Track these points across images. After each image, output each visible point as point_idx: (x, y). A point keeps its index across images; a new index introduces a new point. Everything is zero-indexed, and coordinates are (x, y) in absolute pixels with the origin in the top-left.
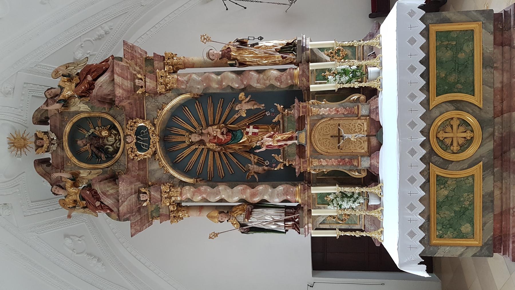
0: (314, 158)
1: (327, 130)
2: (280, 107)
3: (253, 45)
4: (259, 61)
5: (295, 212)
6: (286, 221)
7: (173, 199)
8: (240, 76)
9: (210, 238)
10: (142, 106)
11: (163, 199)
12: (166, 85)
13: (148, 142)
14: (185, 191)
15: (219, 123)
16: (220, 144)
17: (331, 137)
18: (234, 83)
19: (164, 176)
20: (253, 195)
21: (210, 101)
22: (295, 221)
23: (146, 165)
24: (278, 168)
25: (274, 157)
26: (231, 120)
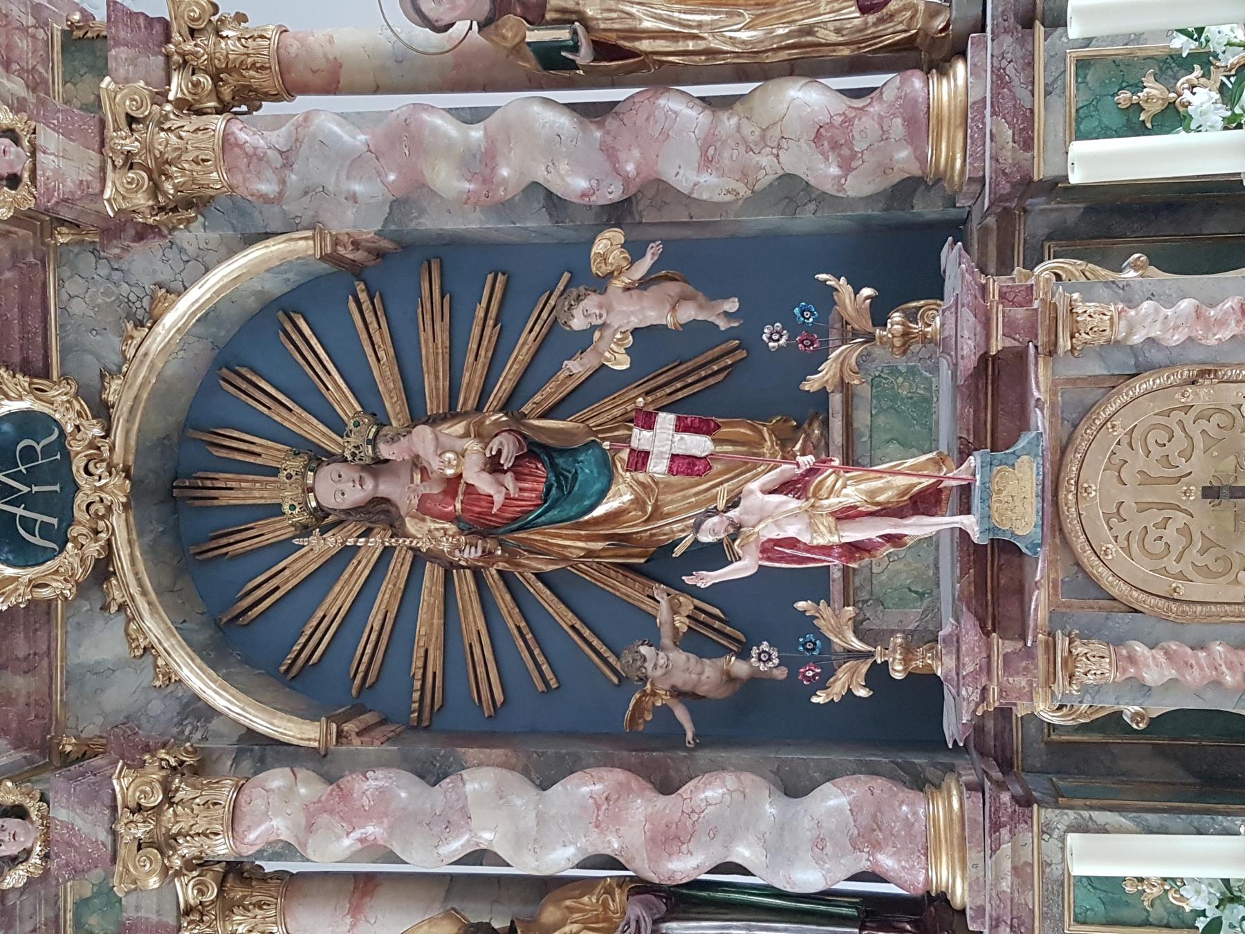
0: (1086, 637)
1: (1173, 449)
2: (853, 300)
4: (714, 29)
7: (187, 849)
8: (601, 125)
10: (35, 299)
11: (122, 852)
12: (158, 172)
13: (63, 506)
14: (259, 804)
15: (479, 408)
16: (479, 524)
17: (1210, 493)
18: (564, 167)
19: (156, 707)
20: (668, 839)
21: (431, 288)
23: (50, 640)
26: (550, 393)
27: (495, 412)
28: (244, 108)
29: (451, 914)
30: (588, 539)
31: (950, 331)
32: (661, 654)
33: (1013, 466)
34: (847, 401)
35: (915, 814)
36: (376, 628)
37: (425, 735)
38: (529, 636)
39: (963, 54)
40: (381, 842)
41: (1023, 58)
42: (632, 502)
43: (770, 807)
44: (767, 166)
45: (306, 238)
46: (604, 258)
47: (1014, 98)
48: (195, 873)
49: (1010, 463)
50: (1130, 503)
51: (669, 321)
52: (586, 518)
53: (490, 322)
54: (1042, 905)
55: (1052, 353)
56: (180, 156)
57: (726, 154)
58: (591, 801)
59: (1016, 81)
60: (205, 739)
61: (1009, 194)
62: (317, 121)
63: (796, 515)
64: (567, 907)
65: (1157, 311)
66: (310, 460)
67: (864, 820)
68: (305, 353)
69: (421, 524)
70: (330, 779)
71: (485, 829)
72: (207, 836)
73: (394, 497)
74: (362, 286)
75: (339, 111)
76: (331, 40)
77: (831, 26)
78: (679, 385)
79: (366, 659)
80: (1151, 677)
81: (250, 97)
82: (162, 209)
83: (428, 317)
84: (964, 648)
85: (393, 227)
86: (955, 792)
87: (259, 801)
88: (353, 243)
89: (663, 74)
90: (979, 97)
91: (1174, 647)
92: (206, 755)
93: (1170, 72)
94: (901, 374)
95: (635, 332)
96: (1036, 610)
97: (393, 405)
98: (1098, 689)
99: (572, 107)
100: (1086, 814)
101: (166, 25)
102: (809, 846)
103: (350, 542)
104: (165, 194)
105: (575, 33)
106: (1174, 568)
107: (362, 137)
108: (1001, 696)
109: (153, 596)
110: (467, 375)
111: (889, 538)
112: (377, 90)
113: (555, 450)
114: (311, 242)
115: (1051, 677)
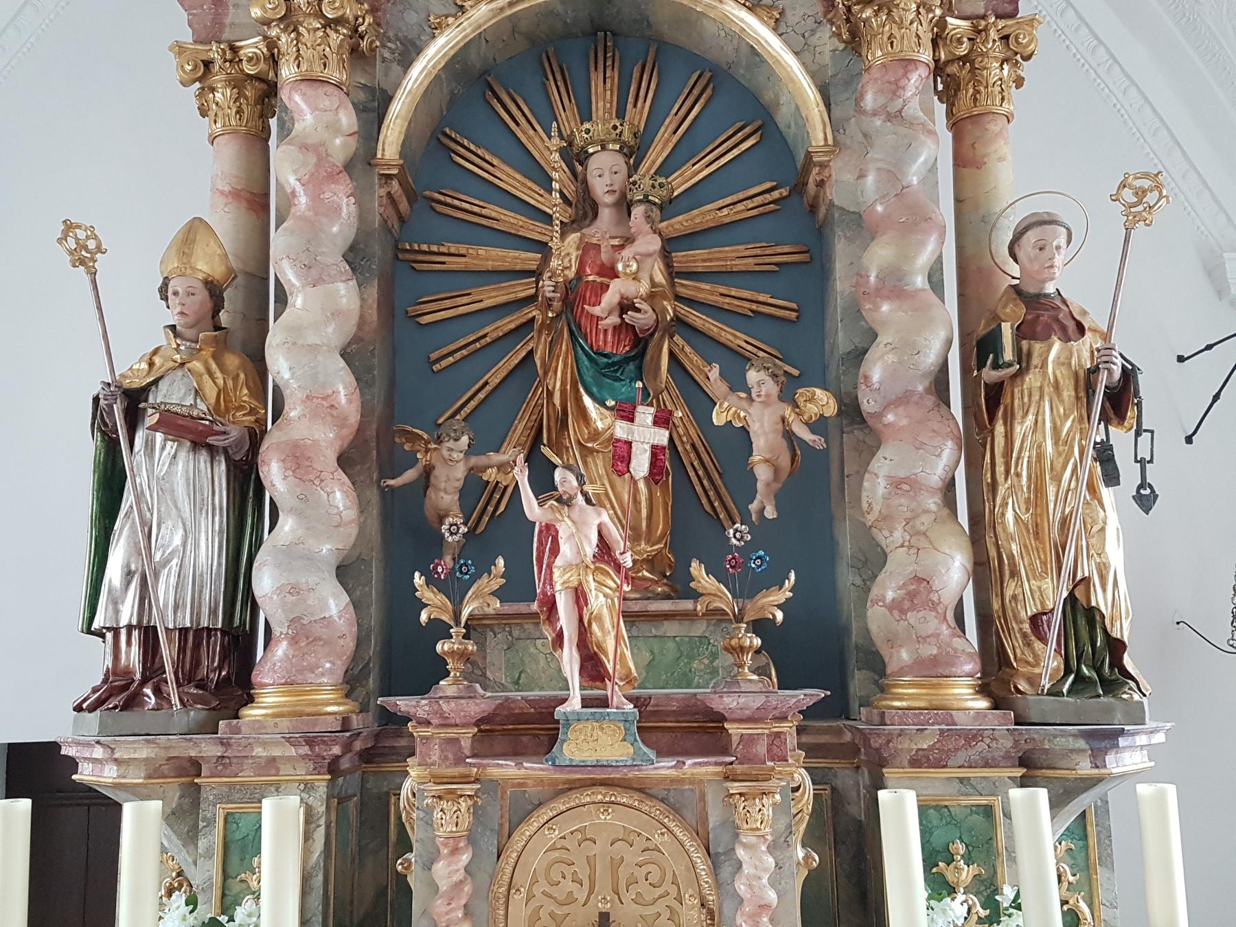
0: (476, 811)
1: (643, 887)
2: (773, 603)
3: (1105, 455)
5: (201, 685)
6: (149, 637)
7: (285, 40)
8: (928, 391)
9: (69, 227)
14: (326, 103)
15: (678, 298)
16: (574, 295)
18: (891, 358)
20: (298, 459)
21: (784, 253)
22: (144, 682)
24: (426, 593)
25: (485, 567)
26: (692, 359)
27: (674, 310)
28: (940, 87)
29: (231, 275)
30: (563, 392)
31: (745, 687)
32: (462, 455)
33: (624, 740)
34: (686, 615)
35: (323, 674)
36: (484, 212)
37: (390, 254)
38: (478, 345)
39: (995, 706)
40: (293, 210)
41: (993, 758)
42: (596, 430)
43: (327, 549)
44: (893, 538)
45: (826, 139)
46: (811, 400)
47: (957, 750)
48: (265, 50)
49: (628, 737)
50: (595, 850)
51: (756, 458)
52: (582, 390)
53: (754, 307)
54: (242, 784)
55: (727, 778)
56: (895, 22)
57: (903, 501)
58: (330, 392)
59: (971, 752)
60: (384, 60)
61: (870, 747)
62: (929, 141)
63: (579, 553)
64: (238, 376)
65: (766, 870)
66: (631, 147)
67: (318, 630)
68: (725, 145)
69: (574, 246)
70: (348, 167)
71: (305, 300)
72: (297, 58)
73: (598, 223)
74: (785, 194)
75: (939, 165)
76: (1001, 159)
77: (1019, 590)
78: (701, 473)
79: (456, 203)
80: (440, 868)
81: (950, 93)
82: (849, 9)
83: (759, 252)
84: (463, 701)
85: (836, 215)
86: (341, 708)
87: (327, 103)
88: (822, 180)
89: (975, 446)
90: (956, 719)
91: (466, 889)
92: (368, 61)
93: (982, 888)
94: (712, 662)
95: (745, 431)
96: (501, 766)
97: (680, 222)
98: (429, 823)
99: (944, 367)
100: (322, 821)
101: (1012, 15)
102: (293, 581)
103: (556, 185)
104: (862, 11)
105: (1010, 365)
106: (537, 890)
107: (915, 181)
108: (422, 738)
109: (508, 12)
110: (708, 287)
111: (560, 636)
112: (958, 201)
113: (642, 362)
114: (822, 143)
115: (438, 779)
